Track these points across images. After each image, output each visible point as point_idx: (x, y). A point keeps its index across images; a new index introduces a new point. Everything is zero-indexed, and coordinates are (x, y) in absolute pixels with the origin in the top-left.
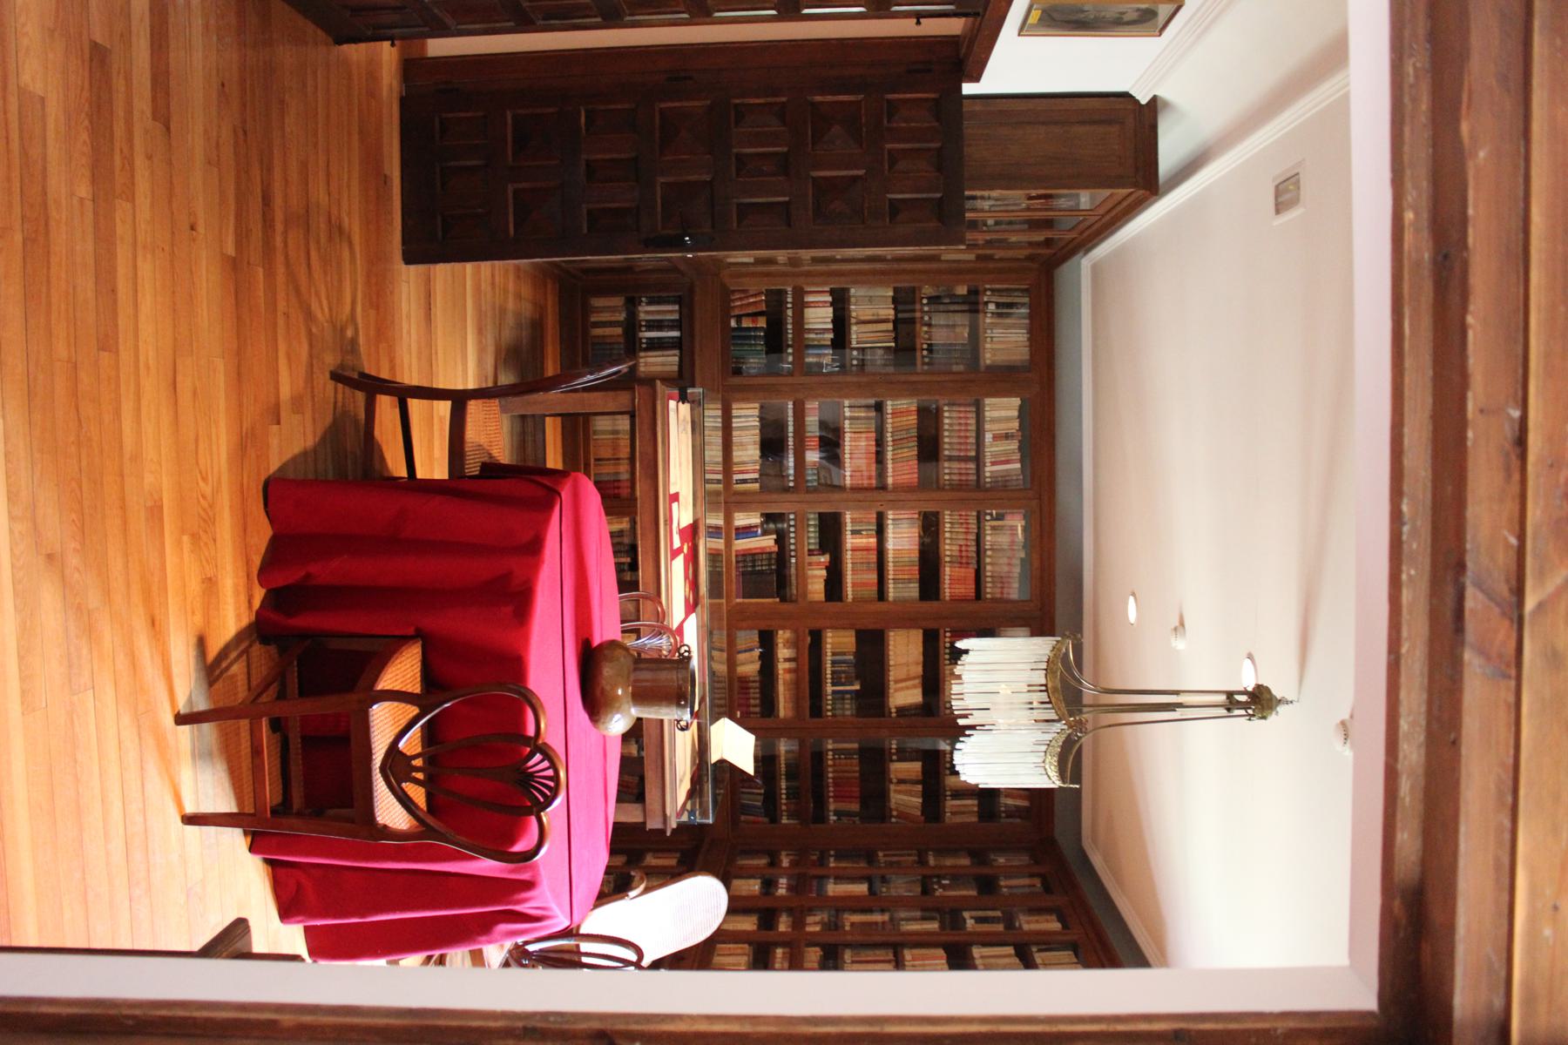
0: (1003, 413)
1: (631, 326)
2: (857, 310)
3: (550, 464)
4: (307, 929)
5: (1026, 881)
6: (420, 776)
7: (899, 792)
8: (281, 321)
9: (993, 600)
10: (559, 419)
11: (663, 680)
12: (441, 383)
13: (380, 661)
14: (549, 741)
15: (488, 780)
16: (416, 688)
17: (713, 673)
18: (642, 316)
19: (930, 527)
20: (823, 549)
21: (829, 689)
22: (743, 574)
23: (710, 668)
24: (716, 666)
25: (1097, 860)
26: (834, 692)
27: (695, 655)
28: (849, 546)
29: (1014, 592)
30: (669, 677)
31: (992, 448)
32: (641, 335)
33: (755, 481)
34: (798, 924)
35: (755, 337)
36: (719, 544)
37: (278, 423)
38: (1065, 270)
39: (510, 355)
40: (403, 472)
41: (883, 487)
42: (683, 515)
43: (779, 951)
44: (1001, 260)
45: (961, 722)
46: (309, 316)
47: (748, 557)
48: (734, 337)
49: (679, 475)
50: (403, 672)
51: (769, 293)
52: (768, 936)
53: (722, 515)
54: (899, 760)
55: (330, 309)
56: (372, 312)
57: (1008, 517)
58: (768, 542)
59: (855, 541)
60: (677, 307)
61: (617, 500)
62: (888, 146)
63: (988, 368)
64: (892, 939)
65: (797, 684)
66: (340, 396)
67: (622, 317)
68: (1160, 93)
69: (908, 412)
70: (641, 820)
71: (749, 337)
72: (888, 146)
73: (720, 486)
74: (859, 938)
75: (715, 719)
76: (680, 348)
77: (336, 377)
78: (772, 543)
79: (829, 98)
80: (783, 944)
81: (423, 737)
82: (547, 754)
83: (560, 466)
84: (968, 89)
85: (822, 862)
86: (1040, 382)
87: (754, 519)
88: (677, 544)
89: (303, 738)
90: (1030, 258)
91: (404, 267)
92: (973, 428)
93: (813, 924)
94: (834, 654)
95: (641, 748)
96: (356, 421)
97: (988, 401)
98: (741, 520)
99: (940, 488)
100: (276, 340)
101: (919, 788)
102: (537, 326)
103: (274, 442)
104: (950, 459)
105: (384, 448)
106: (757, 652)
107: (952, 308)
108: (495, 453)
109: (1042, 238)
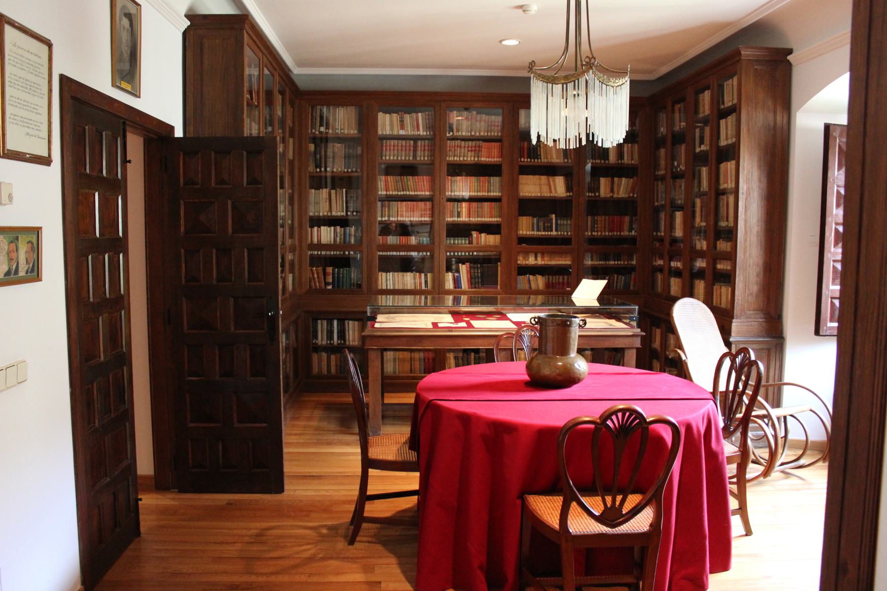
0: (388, 123)
1: (331, 349)
2: (323, 212)
3: (412, 401)
4: (711, 572)
5: (677, 115)
6: (619, 498)
7: (618, 192)
8: (315, 579)
9: (502, 130)
10: (386, 394)
11: (553, 335)
12: (359, 470)
13: (538, 525)
14: (598, 416)
15: (622, 454)
16: (559, 500)
17: (543, 304)
18: (324, 343)
19: (457, 170)
20: (469, 235)
21: (554, 233)
22: (483, 284)
23: (540, 306)
24: (539, 302)
25: (664, 70)
26: (556, 230)
27: (533, 315)
28: (467, 219)
29: (497, 119)
30: (551, 331)
31: (408, 131)
32: (335, 343)
33: (426, 276)
34: (701, 254)
35: (338, 274)
36: (464, 299)
37: (380, 582)
38: (301, 84)
39: (344, 426)
40: (414, 499)
41: (430, 199)
42: (446, 320)
43: (719, 266)
44: (293, 122)
45: (584, 143)
46: (311, 559)
47: (472, 281)
48: (338, 287)
49: (422, 322)
50: (547, 509)
51: (312, 265)
52: (709, 275)
53: (446, 297)
54: (599, 192)
55: (309, 544)
56: (313, 515)
57: (451, 121)
58: (464, 268)
59: (464, 215)
60: (319, 321)
61: (436, 362)
62: (213, 185)
63: (359, 131)
64: (713, 195)
65: (552, 254)
66: (365, 539)
67: (324, 355)
68: (183, 11)
69: (386, 181)
70: (634, 351)
71: (338, 277)
72: (213, 185)
73: (429, 297)
74: (712, 217)
75: (572, 303)
76: (344, 320)
77: (352, 542)
78: (464, 266)
79: (182, 222)
80: (715, 264)
81: (589, 496)
82: (607, 416)
83: (414, 395)
84: (179, 133)
85: (661, 240)
86: (369, 100)
87: (449, 276)
88: (464, 324)
89: (587, 574)
90: (292, 104)
91: (286, 493)
92: (396, 141)
93: (702, 244)
94: (533, 230)
95: (587, 350)
96: (381, 528)
97: (380, 133)
98: (449, 285)
99: (432, 163)
100: (324, 583)
101: (616, 179)
102: (329, 407)
103: (392, 586)
104: (415, 156)
105: (399, 509)
106: (531, 277)
107: (323, 154)
108: (403, 440)
109: (280, 97)
